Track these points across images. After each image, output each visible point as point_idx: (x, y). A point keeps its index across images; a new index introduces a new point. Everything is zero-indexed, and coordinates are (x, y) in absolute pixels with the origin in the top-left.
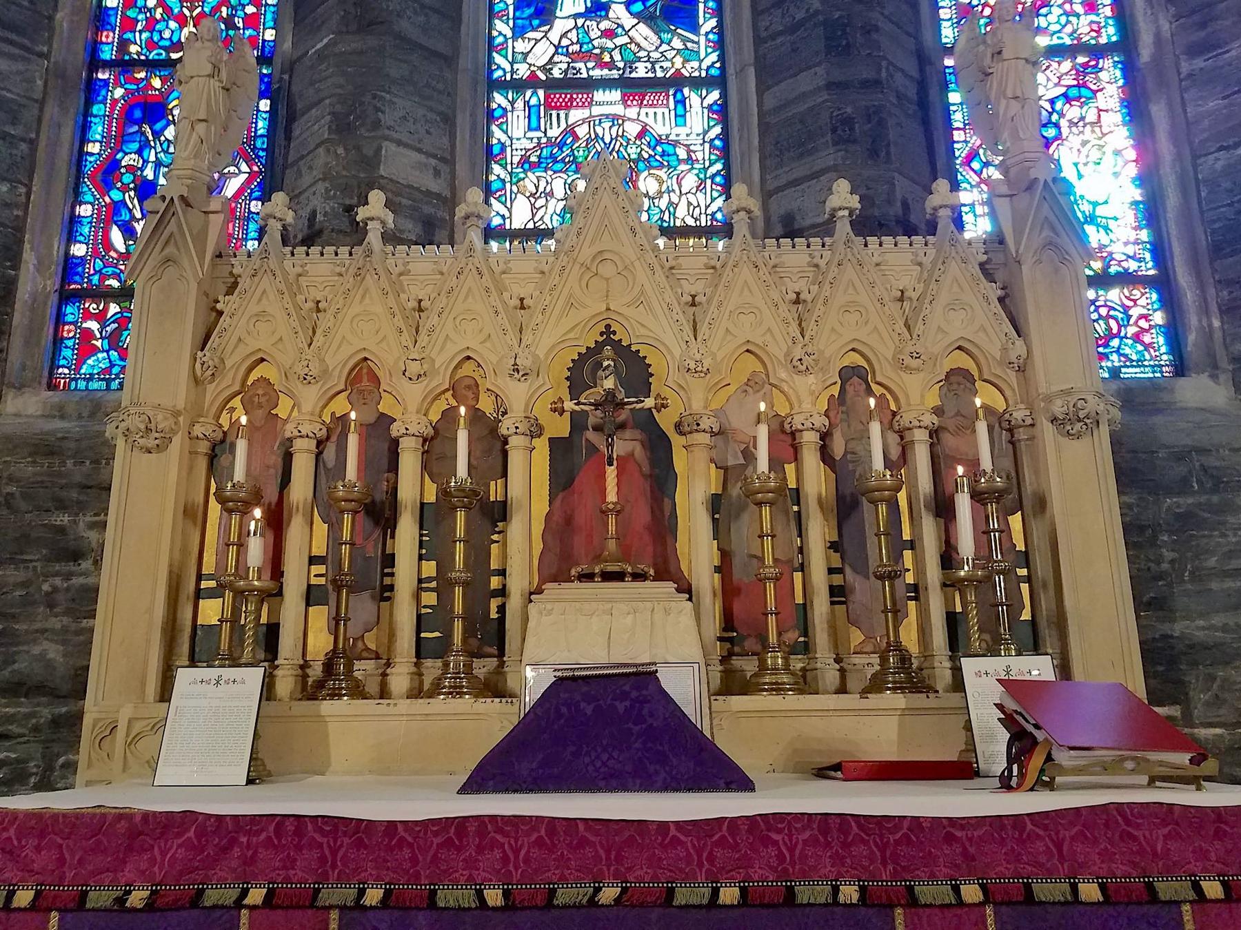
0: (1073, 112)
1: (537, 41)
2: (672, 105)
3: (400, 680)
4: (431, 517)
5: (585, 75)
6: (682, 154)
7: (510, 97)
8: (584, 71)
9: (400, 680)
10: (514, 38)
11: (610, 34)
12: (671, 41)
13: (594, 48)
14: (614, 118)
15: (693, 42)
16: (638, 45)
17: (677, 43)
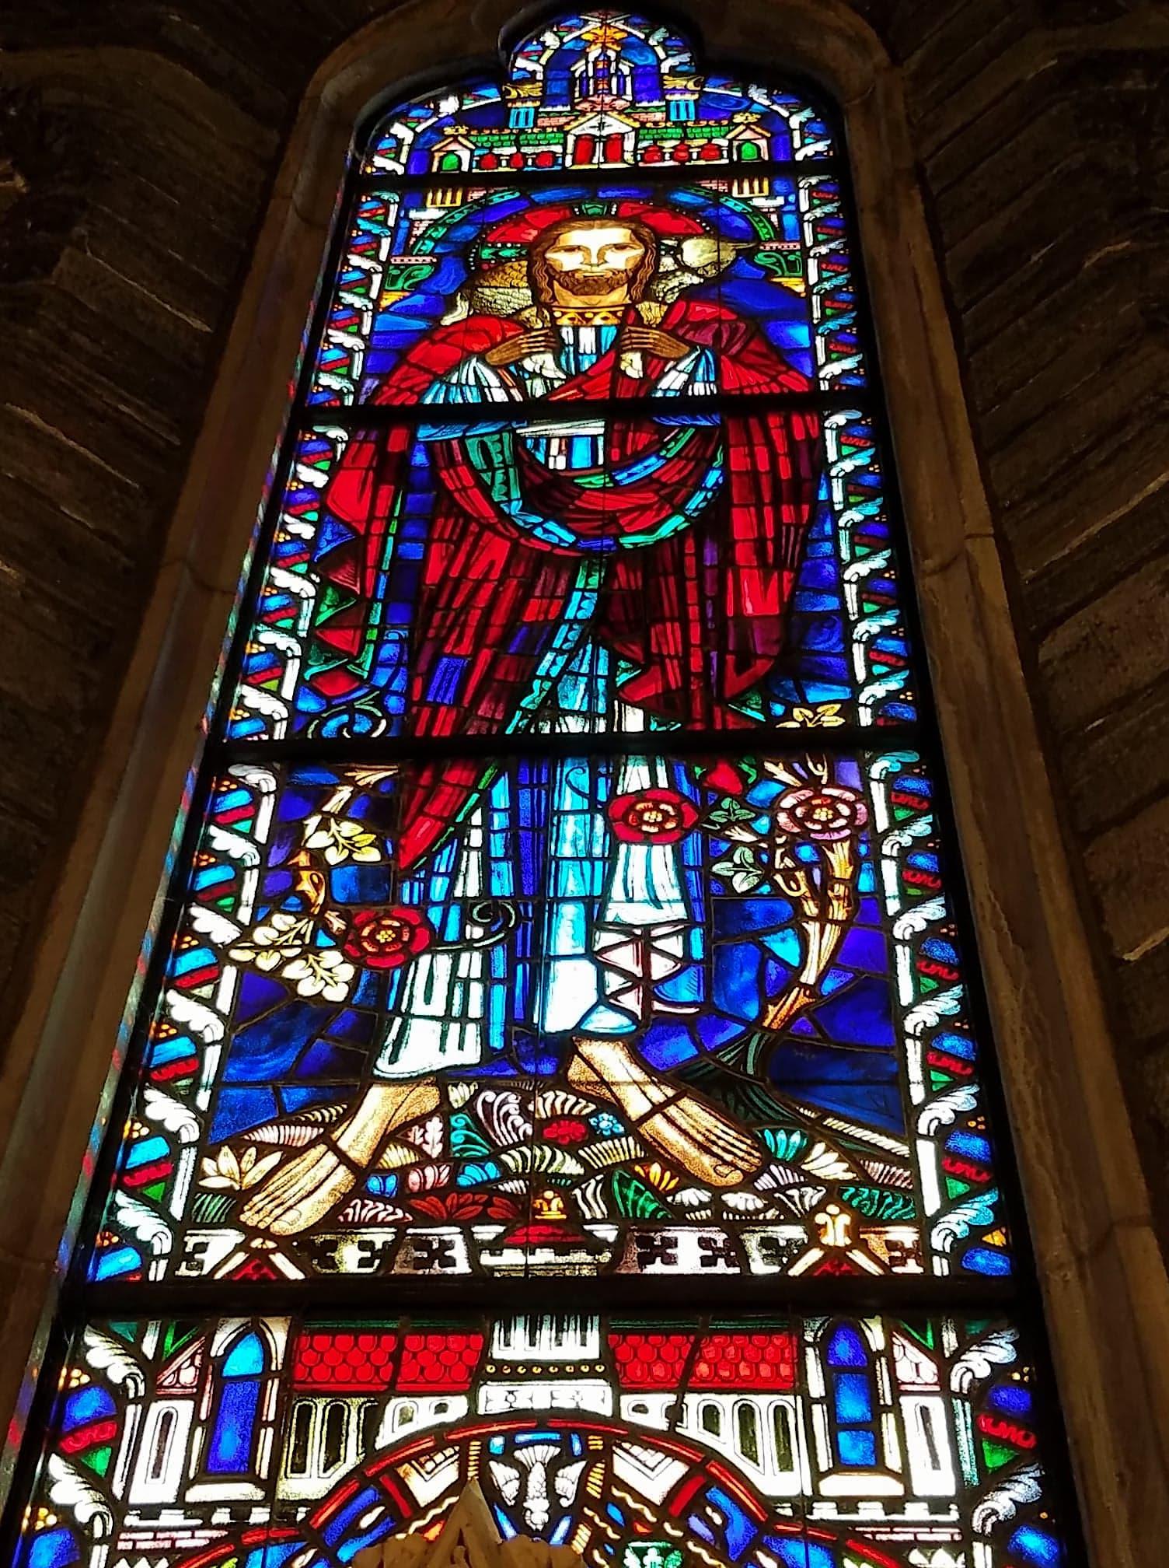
1: (291, 1153)
2: (816, 1386)
5: (462, 1267)
7: (149, 1347)
8: (459, 1252)
10: (207, 1148)
11: (571, 1134)
12: (803, 1153)
13: (507, 1175)
14: (566, 1426)
15: (888, 1157)
16: (674, 1166)
17: (827, 1164)
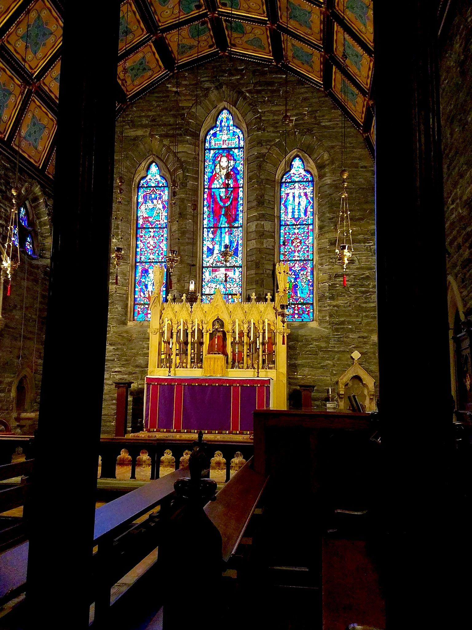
0: (302, 273)
3: (189, 366)
4: (193, 344)
6: (234, 280)
9: (189, 366)
17: (234, 259)
